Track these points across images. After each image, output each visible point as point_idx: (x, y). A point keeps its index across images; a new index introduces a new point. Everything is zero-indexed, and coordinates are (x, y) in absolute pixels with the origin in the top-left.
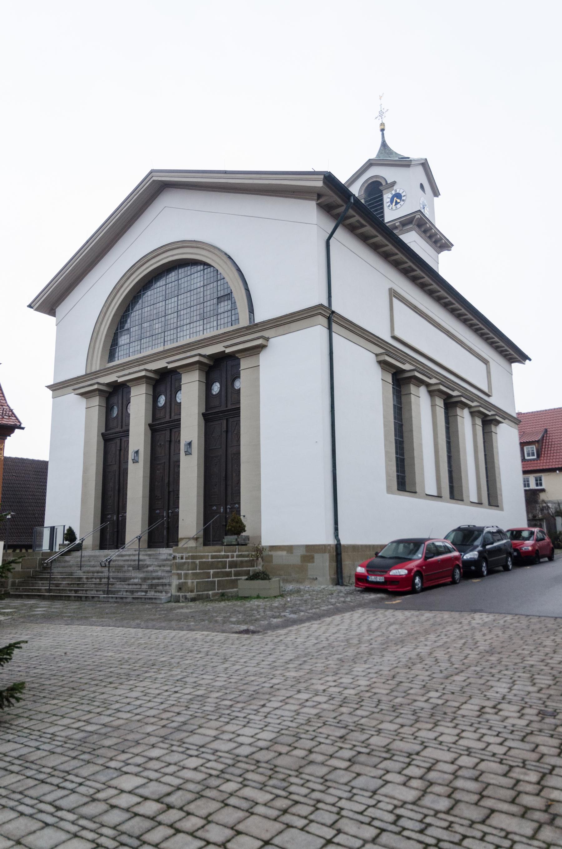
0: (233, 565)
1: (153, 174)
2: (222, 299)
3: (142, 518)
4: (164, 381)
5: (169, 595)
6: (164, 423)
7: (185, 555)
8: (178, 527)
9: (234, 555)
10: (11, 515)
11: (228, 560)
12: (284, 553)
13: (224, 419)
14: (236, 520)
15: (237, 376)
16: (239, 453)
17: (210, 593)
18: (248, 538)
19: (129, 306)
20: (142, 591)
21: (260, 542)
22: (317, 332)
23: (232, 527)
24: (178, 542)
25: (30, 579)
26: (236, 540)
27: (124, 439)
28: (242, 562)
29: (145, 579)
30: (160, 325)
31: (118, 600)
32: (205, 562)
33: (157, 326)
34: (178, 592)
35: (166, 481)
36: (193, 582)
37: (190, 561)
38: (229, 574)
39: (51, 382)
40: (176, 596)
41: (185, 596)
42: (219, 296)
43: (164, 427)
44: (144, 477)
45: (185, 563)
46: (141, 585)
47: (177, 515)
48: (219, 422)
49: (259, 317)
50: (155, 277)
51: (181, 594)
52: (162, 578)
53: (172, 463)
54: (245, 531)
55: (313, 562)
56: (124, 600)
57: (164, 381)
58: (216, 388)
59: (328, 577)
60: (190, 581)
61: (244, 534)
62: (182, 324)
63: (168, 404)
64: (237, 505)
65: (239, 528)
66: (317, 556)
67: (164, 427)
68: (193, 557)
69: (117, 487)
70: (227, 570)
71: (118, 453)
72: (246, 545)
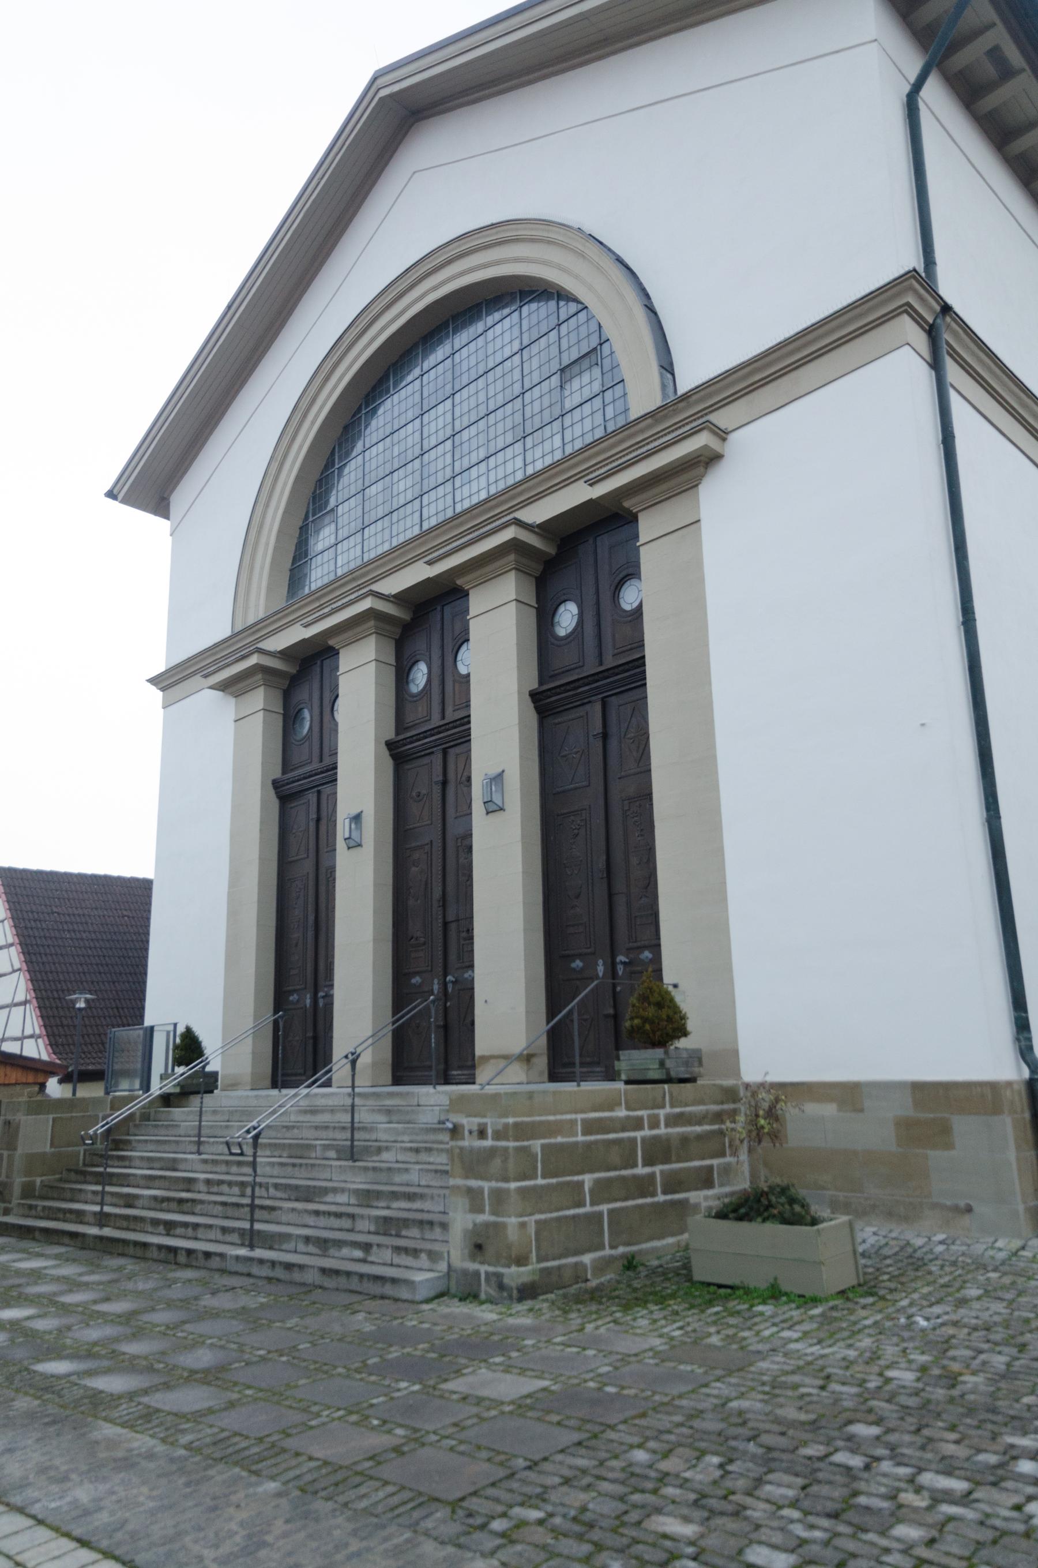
0: (658, 1151)
1: (380, 82)
2: (576, 369)
3: (374, 1001)
4: (425, 620)
5: (443, 1266)
6: (426, 734)
7: (491, 1123)
8: (473, 1023)
9: (659, 1117)
10: (87, 1001)
11: (639, 1135)
12: (829, 1109)
13: (596, 702)
14: (656, 998)
15: (631, 572)
16: (646, 796)
17: (587, 1259)
18: (696, 1057)
19: (333, 453)
20: (355, 1245)
21: (737, 1073)
22: (896, 373)
23: (645, 1020)
24: (473, 1067)
25: (73, 1176)
26: (662, 1064)
27: (326, 790)
28: (685, 1140)
29: (367, 1197)
30: (409, 482)
31: (279, 1273)
32: (562, 1147)
33: (402, 486)
34: (473, 1258)
35: (437, 893)
36: (523, 1225)
37: (512, 1144)
38: (643, 1186)
39: (159, 667)
40: (465, 1273)
41: (499, 1276)
42: (566, 362)
43: (427, 747)
44: (376, 885)
45: (492, 1152)
46: (352, 1217)
47: (468, 991)
48: (581, 712)
49: (693, 371)
50: (394, 364)
51: (483, 1269)
52: (422, 1197)
53: (450, 844)
54: (685, 1034)
55: (949, 1146)
56: (297, 1276)
57: (425, 620)
58: (567, 618)
59: (1021, 1208)
60: (513, 1221)
61: (682, 1043)
62: (466, 465)
63: (436, 683)
64: (647, 955)
65: (664, 1024)
66: (963, 1125)
67: (427, 747)
68: (522, 1131)
69: (311, 918)
70: (641, 1170)
71: (312, 825)
72: (692, 1080)
